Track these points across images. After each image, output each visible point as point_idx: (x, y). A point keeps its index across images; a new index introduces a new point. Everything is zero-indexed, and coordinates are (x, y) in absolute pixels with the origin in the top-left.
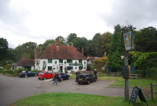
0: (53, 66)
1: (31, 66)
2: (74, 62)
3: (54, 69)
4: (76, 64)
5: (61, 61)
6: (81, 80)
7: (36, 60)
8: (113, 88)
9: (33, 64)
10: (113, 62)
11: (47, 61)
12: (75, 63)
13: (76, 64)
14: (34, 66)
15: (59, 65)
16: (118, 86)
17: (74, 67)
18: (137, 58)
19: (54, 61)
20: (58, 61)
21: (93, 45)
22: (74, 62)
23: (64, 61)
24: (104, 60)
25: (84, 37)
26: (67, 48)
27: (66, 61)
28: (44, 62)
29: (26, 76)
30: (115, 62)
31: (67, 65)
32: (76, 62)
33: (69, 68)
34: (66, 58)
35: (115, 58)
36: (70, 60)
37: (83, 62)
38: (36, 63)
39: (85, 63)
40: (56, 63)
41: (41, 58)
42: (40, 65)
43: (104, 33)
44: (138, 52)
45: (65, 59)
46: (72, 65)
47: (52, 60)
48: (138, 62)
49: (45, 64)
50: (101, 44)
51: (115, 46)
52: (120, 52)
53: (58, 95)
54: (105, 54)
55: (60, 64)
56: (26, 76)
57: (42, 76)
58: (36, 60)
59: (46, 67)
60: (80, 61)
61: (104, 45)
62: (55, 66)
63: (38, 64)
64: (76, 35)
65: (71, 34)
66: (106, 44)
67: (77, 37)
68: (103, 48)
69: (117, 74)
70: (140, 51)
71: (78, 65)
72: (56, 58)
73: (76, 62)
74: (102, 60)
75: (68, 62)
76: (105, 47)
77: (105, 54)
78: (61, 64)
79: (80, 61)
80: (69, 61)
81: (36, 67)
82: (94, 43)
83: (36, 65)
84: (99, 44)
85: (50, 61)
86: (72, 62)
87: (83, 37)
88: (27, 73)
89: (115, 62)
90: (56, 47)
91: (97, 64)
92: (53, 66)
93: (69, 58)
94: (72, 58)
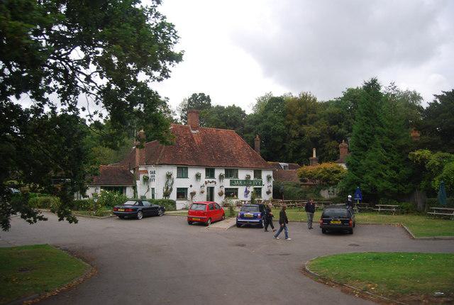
0: (191, 186)
1: (125, 188)
2: (242, 175)
3: (193, 194)
4: (247, 182)
5: (210, 173)
6: (337, 222)
7: (140, 169)
8: (435, 239)
9: (131, 181)
10: (368, 177)
11: (174, 171)
12: (244, 179)
13: (247, 182)
14: (135, 188)
15: (206, 183)
16: (443, 234)
17: (241, 190)
18: (441, 168)
19: (192, 172)
20: (203, 172)
21: (267, 128)
22: (242, 175)
23: (218, 173)
24: (328, 171)
25: (237, 106)
26: (218, 137)
27: (223, 172)
28: (169, 176)
29: (140, 215)
30: (376, 177)
31: (227, 183)
32: (249, 177)
33: (231, 193)
34: (224, 164)
35: (375, 167)
36: (231, 170)
37: (264, 174)
38: (141, 176)
39: (269, 178)
40: (198, 177)
41: (161, 165)
42: (152, 185)
43: (255, 102)
44: (440, 153)
45: (220, 167)
46: (237, 185)
47: (187, 169)
48: (447, 177)
49: (170, 182)
50: (288, 126)
51: (369, 134)
52: (387, 151)
53: (376, 259)
54: (314, 156)
55: (207, 180)
56: (140, 215)
57: (203, 214)
58: (140, 169)
59: (171, 190)
60: (258, 174)
61: (296, 129)
62: (196, 187)
63: (146, 180)
64: (208, 99)
65: (194, 95)
66: (305, 127)
67: (214, 103)
68: (295, 139)
69: (389, 207)
70: (444, 151)
71: (252, 183)
72: (199, 166)
73: (249, 177)
74: (323, 172)
75: (227, 176)
76: (301, 135)
77: (314, 156)
78: (211, 180)
79: (258, 174)
80: (230, 173)
81: (142, 190)
82: (272, 124)
83: (139, 183)
84: (284, 127)
85: (183, 173)
86: (237, 176)
87: (232, 105)
88: (140, 208)
89: (376, 177)
90: (191, 134)
91: (305, 181)
92: (191, 186)
93: (230, 165)
94: (238, 165)
